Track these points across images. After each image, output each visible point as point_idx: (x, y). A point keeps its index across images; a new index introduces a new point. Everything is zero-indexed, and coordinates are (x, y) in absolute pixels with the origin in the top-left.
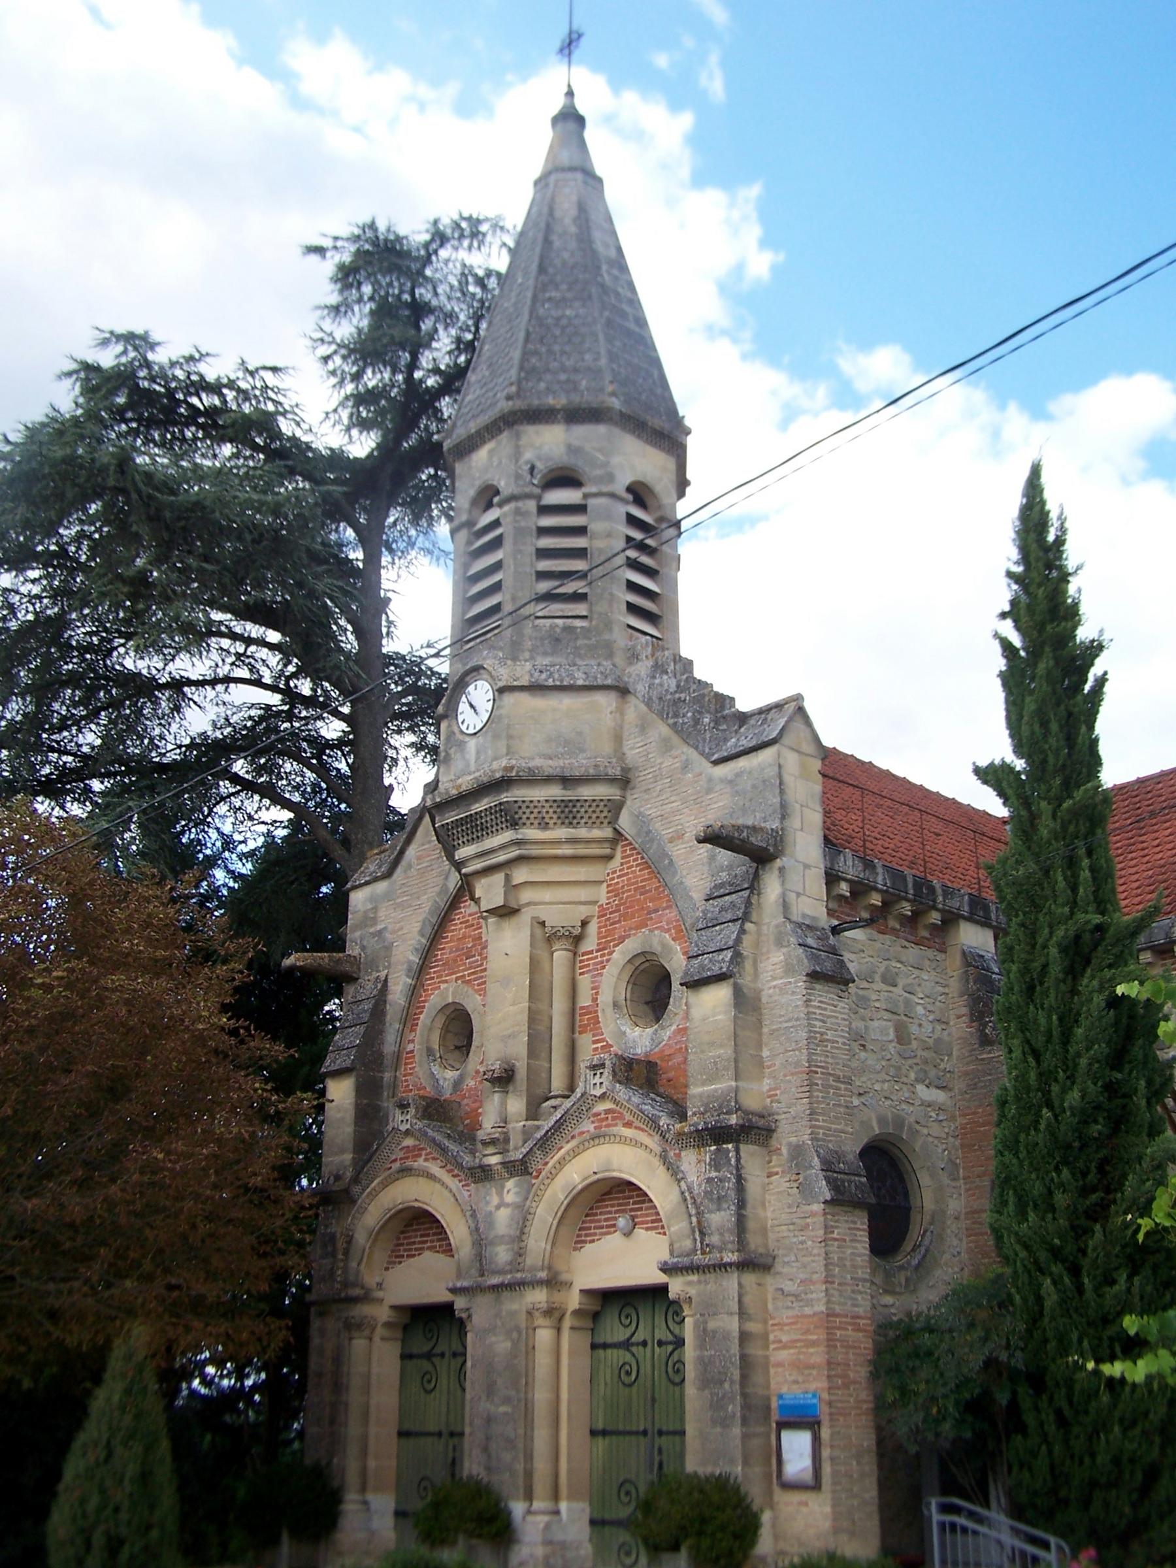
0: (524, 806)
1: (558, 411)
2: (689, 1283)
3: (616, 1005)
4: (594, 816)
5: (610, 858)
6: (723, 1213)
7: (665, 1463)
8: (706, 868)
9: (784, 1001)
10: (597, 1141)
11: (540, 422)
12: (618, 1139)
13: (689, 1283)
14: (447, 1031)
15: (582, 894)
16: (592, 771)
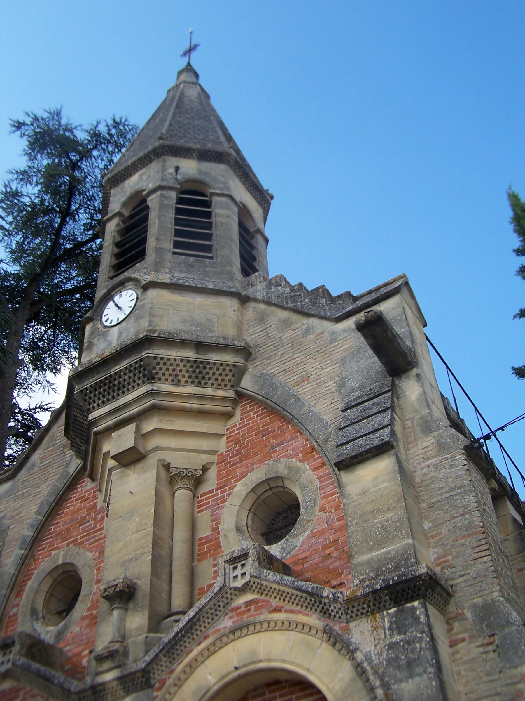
0: (161, 363)
1: (194, 150)
3: (238, 529)
4: (220, 378)
5: (229, 416)
6: (417, 679)
8: (336, 395)
9: (441, 476)
10: (238, 634)
11: (180, 157)
12: (265, 625)
14: (52, 595)
15: (205, 444)
16: (221, 341)
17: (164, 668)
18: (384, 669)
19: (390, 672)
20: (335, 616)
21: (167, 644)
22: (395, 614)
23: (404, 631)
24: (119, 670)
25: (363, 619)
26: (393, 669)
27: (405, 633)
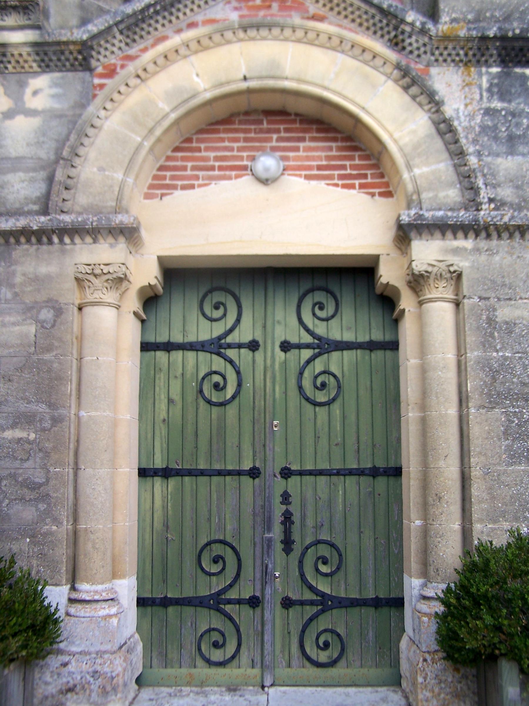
2: (456, 251)
7: (296, 518)
13: (456, 251)
17: (115, 49)
18: (476, 135)
19: (483, 141)
20: (411, 52)
21: (129, 16)
22: (499, 75)
23: (508, 98)
24: (37, 32)
25: (451, 68)
26: (488, 140)
27: (510, 101)
